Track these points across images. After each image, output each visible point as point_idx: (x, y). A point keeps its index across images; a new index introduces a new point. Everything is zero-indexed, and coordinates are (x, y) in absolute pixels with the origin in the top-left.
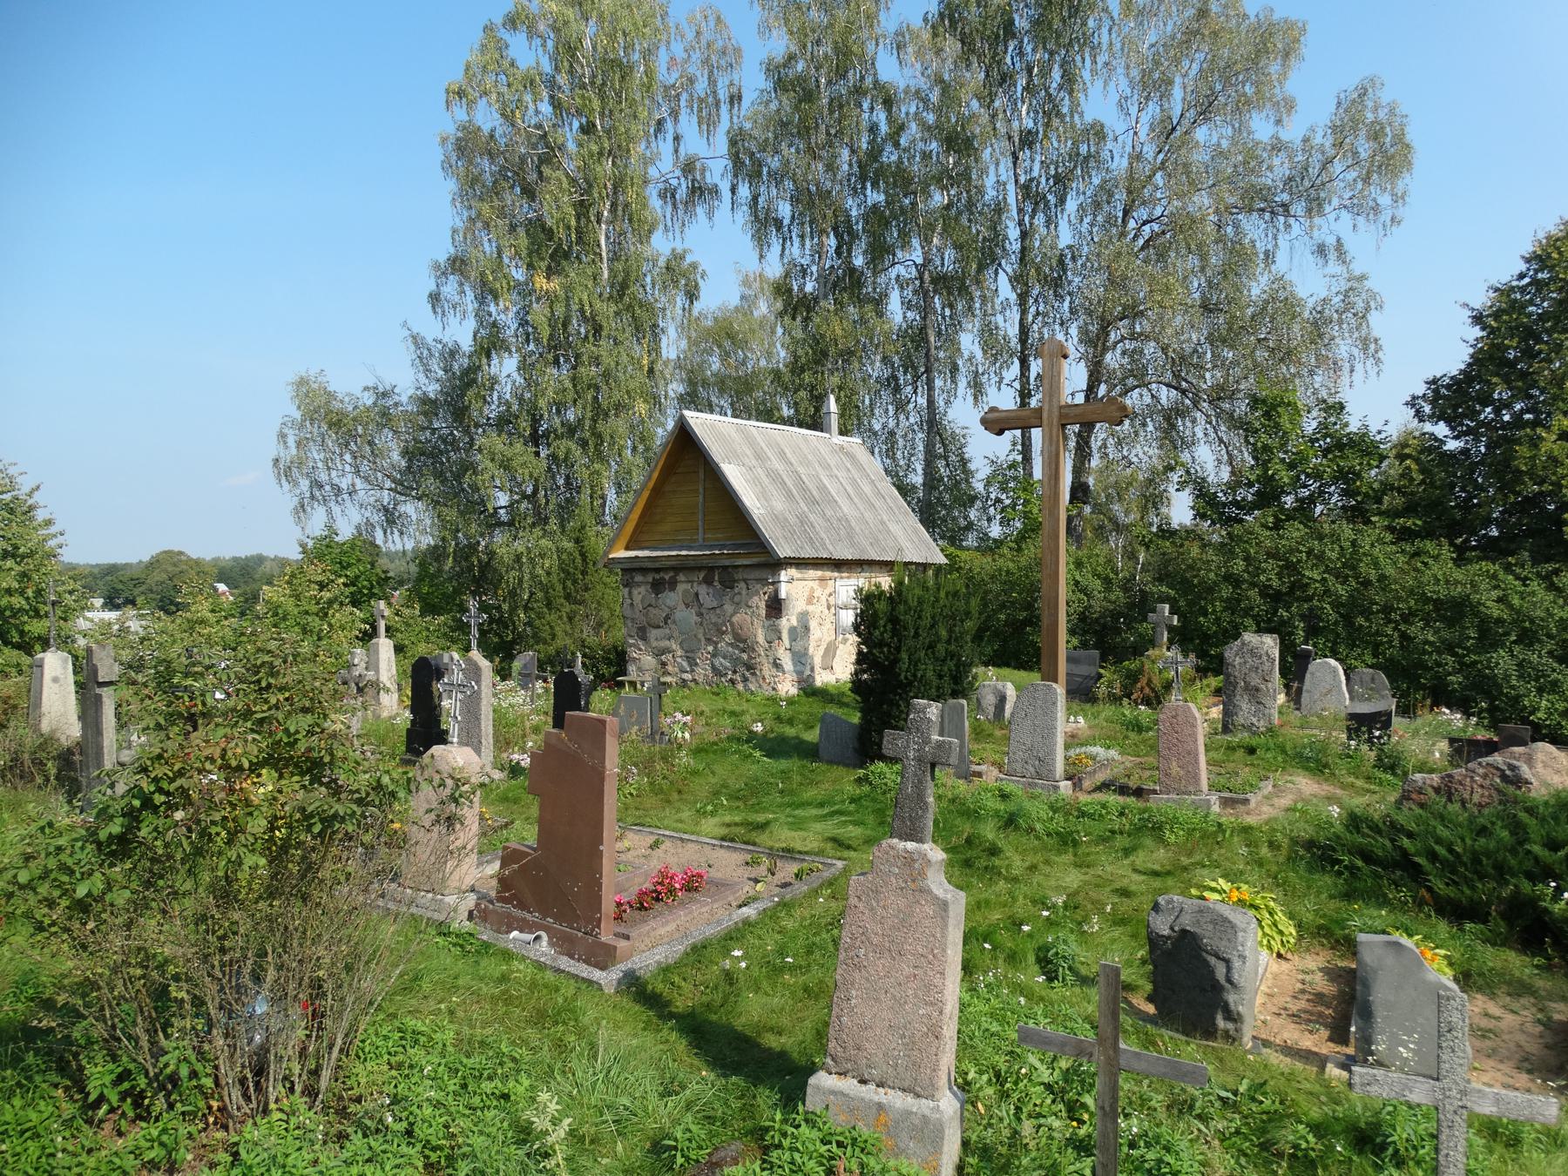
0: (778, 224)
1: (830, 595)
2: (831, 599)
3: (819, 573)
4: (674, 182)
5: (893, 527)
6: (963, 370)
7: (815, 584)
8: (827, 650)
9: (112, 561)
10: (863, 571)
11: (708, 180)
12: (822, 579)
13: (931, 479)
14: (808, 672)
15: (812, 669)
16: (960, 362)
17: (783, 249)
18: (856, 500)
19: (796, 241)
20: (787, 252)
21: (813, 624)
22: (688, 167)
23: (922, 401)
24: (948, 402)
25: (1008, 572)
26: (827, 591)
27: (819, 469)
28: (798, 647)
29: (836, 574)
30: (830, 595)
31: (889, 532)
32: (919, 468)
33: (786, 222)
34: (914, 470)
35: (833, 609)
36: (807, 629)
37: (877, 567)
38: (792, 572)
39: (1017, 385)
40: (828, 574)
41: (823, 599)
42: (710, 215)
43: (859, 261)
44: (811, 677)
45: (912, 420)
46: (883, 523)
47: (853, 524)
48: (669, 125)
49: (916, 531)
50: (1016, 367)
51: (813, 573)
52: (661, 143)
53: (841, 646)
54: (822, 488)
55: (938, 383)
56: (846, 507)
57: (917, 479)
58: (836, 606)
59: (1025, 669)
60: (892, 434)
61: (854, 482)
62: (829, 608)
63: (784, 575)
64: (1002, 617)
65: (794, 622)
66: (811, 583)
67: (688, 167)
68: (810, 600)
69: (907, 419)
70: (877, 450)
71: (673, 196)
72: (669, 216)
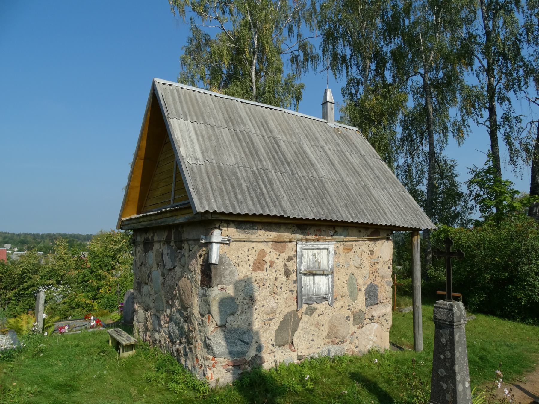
0: (344, 58)
1: (290, 259)
2: (292, 266)
3: (273, 234)
4: (297, 53)
5: (377, 193)
6: (450, 128)
7: (268, 248)
8: (284, 324)
9: (89, 233)
10: (336, 233)
11: (314, 51)
12: (276, 242)
13: (431, 187)
14: (253, 352)
15: (259, 349)
16: (449, 125)
17: (347, 73)
18: (338, 167)
19: (354, 67)
20: (349, 72)
21: (260, 295)
22: (303, 47)
23: (427, 149)
24: (442, 148)
25: (490, 242)
26: (285, 255)
27: (304, 140)
28: (234, 322)
29: (299, 236)
30: (290, 259)
31: (371, 196)
32: (425, 182)
33: (348, 58)
34: (422, 183)
35: (293, 277)
36: (252, 299)
37: (355, 231)
38: (232, 232)
39: (488, 123)
40: (287, 235)
41: (279, 264)
42: (315, 68)
43: (388, 75)
44: (257, 360)
45: (421, 159)
46: (365, 187)
47: (328, 185)
48: (295, 29)
49: (402, 198)
50: (486, 114)
51: (262, 234)
52: (292, 38)
53: (305, 318)
54: (301, 154)
55: (436, 137)
56: (324, 171)
57: (423, 188)
58: (299, 273)
59: (509, 319)
60: (409, 166)
61: (341, 154)
62: (287, 274)
63: (217, 236)
64: (488, 276)
65: (230, 291)
66: (261, 246)
67: (303, 47)
68: (259, 265)
69: (419, 158)
70: (400, 176)
71: (296, 60)
72: (294, 69)
